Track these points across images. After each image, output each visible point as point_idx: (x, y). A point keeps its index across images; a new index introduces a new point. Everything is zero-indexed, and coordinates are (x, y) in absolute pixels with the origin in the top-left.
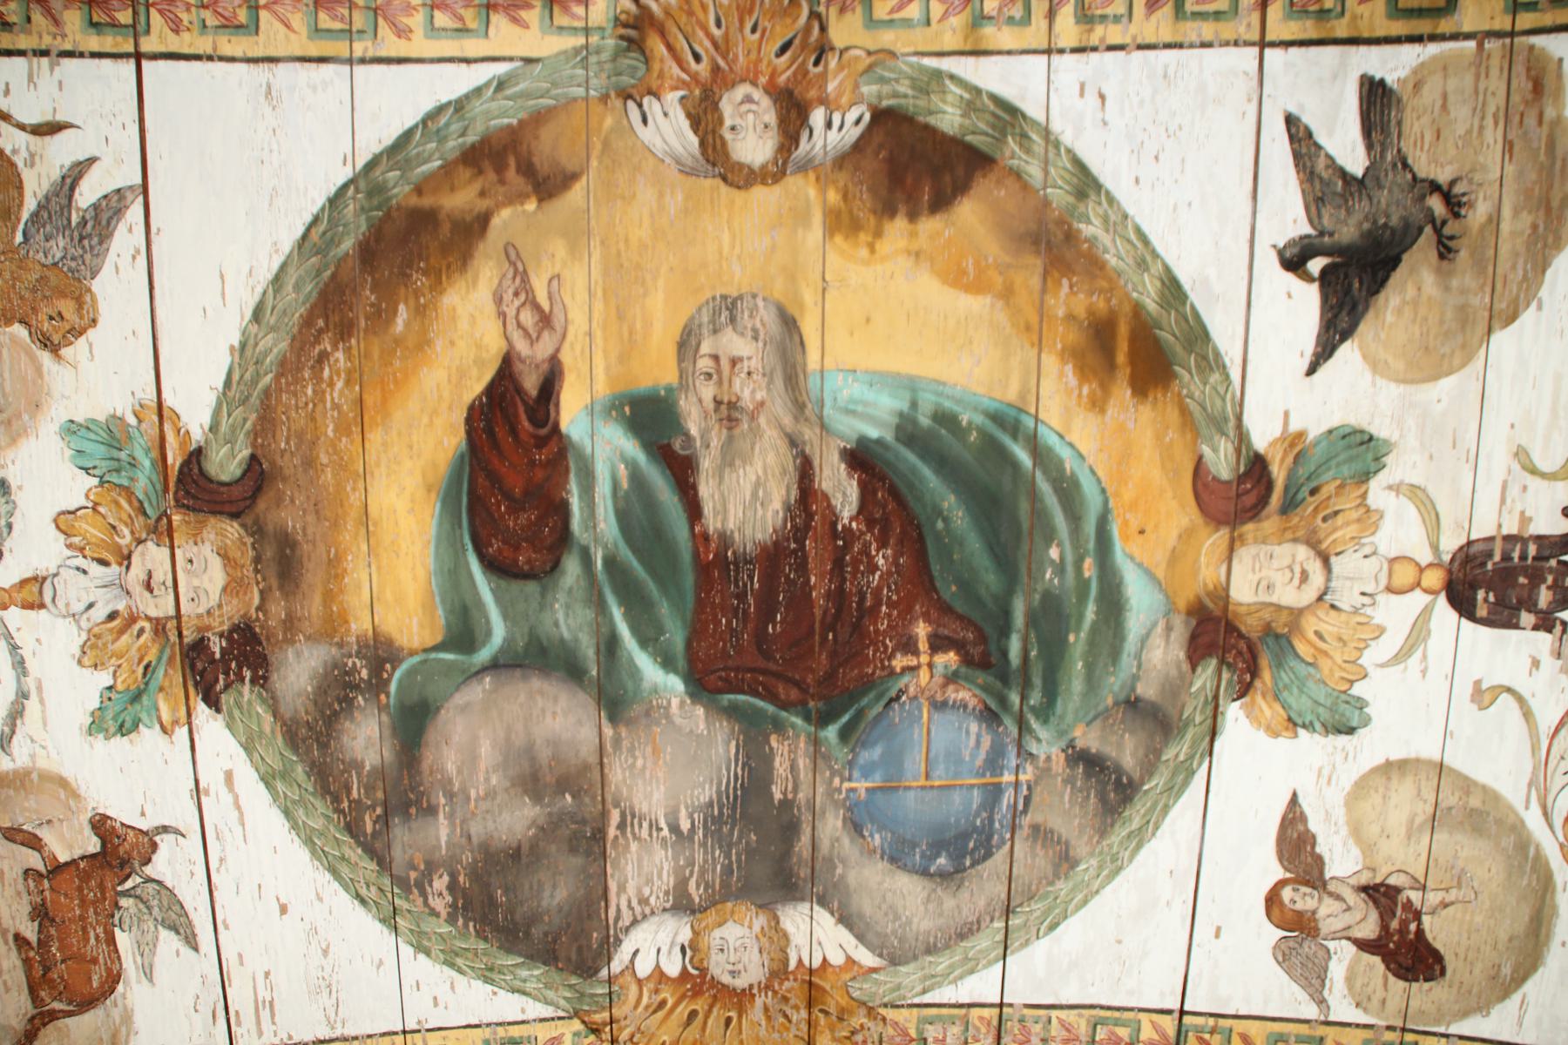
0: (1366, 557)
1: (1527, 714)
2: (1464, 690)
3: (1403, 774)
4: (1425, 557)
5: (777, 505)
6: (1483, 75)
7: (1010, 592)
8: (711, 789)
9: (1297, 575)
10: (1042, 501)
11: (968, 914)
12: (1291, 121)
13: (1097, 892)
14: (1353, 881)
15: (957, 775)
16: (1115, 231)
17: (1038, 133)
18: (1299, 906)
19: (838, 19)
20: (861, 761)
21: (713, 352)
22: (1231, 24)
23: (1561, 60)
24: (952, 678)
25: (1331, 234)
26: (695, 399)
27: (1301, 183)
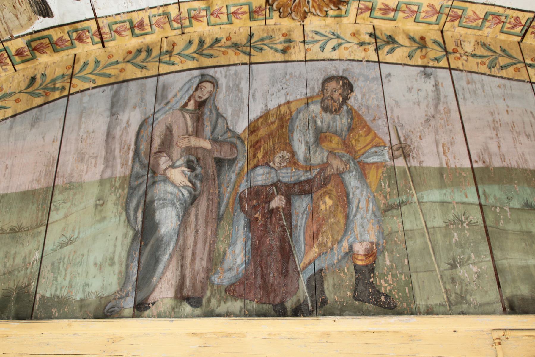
6: (6, 28)
19: (262, 4)
22: (110, 22)
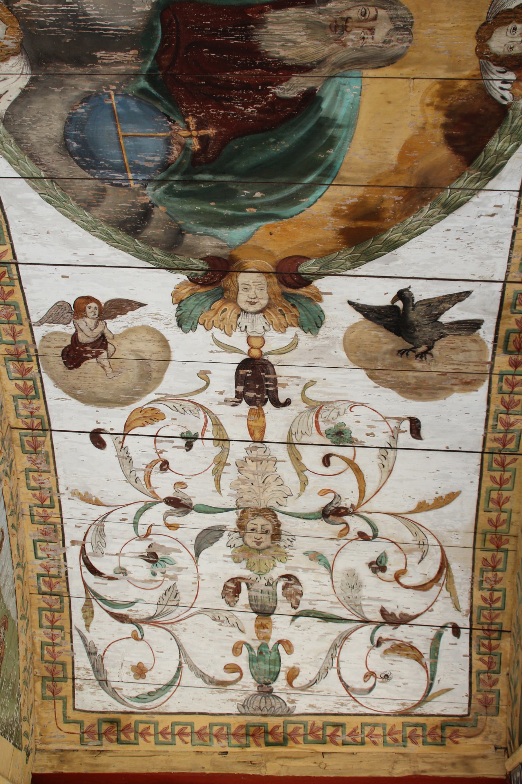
0: (264, 327)
1: (198, 391)
2: (206, 367)
3: (162, 347)
4: (265, 350)
5: (282, 53)
7: (235, 174)
8: (96, 14)
9: (253, 301)
10: (286, 188)
11: (45, 159)
12: (467, 294)
13: (74, 221)
14: (106, 331)
15: (128, 151)
16: (424, 221)
17: (480, 186)
18: (88, 310)
20: (128, 101)
21: (378, 17)
23: (477, 391)
24: (184, 147)
25: (413, 310)
26: (350, 6)
27: (438, 298)
